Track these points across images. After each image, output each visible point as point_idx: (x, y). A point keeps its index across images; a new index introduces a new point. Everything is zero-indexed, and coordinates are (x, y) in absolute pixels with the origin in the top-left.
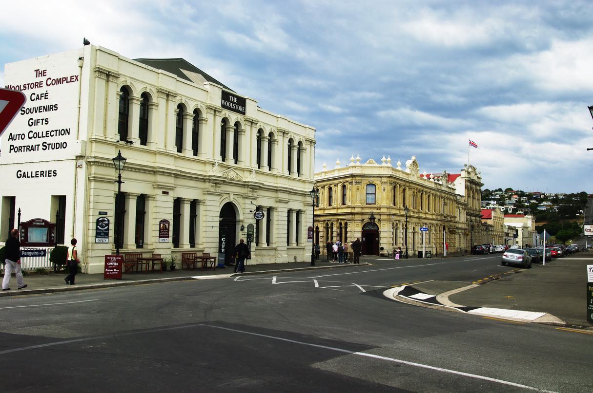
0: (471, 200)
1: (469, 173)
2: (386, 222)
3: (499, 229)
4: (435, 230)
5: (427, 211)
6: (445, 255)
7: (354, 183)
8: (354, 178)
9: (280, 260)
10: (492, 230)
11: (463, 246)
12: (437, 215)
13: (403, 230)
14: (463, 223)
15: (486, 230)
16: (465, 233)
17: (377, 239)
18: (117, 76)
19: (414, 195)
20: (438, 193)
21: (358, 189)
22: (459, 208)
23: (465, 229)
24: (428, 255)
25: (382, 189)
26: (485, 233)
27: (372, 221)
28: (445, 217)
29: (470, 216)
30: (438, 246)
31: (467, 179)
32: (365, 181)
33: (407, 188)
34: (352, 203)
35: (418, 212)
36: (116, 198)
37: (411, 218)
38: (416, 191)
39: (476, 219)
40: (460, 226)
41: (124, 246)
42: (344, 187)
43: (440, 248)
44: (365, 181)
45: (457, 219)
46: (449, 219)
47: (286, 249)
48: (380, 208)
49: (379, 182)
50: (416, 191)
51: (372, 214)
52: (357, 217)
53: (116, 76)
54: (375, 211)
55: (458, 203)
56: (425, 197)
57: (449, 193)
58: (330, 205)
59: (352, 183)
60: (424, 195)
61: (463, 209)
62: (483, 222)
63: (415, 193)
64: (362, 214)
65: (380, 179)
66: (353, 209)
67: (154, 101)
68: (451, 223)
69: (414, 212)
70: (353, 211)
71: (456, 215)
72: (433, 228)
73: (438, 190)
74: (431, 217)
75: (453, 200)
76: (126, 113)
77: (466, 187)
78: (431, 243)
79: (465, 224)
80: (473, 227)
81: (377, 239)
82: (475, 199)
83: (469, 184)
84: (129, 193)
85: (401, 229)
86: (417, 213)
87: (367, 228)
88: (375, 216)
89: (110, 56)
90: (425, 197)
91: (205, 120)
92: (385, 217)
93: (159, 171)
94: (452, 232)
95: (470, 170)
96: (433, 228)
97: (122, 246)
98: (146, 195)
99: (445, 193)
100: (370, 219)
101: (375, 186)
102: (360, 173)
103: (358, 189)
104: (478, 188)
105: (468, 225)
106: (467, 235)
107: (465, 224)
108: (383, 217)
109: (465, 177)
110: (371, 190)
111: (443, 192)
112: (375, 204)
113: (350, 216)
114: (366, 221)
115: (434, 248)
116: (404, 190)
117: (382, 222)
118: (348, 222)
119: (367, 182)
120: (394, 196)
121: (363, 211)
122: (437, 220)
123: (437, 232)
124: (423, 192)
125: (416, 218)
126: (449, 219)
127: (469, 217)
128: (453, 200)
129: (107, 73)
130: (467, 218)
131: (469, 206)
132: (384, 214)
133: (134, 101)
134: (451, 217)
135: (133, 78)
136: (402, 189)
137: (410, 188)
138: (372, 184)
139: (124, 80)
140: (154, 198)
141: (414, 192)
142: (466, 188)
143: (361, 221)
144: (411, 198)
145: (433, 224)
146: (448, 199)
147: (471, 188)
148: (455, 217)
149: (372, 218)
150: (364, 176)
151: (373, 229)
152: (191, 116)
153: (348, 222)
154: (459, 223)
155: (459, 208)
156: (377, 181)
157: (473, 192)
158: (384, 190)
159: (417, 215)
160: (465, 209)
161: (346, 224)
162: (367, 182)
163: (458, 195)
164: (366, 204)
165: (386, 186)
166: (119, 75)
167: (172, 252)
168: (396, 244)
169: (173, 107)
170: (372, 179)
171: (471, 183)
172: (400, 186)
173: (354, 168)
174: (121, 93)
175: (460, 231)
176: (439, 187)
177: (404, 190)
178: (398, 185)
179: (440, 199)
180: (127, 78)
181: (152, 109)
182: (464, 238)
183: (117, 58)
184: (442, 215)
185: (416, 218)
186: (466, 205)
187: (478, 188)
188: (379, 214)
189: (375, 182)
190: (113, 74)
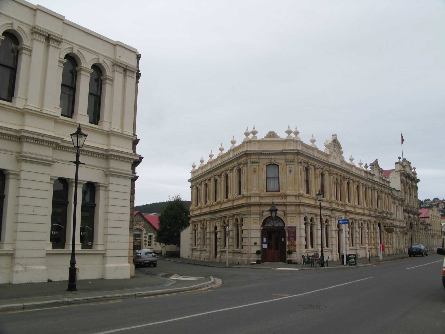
0: (407, 196)
1: (404, 167)
2: (295, 215)
3: (438, 228)
4: (368, 228)
5: (356, 204)
6: (381, 257)
7: (249, 164)
8: (249, 157)
9: (21, 277)
10: (430, 230)
11: (402, 247)
12: (370, 210)
13: (349, 229)
14: (401, 221)
15: (425, 229)
16: (404, 232)
17: (283, 239)
18: (60, 40)
19: (338, 183)
20: (370, 185)
21: (255, 172)
22: (395, 203)
23: (403, 228)
24: (352, 260)
25: (288, 169)
26: (424, 232)
27: (274, 215)
28: (379, 213)
29: (408, 213)
30: (373, 247)
31: (402, 172)
32: (264, 161)
33: (327, 173)
34: (247, 191)
35: (345, 205)
36: (54, 185)
37: (334, 212)
38: (339, 178)
39: (414, 217)
40: (398, 224)
41: (65, 245)
42: (240, 171)
43: (375, 250)
44: (264, 161)
45: (393, 216)
46: (385, 215)
47: (44, 256)
48: (286, 197)
49: (282, 162)
50: (339, 178)
51: (273, 205)
52: (253, 209)
53: (59, 41)
54: (276, 201)
55: (395, 198)
56: (353, 187)
57: (383, 186)
58: (240, 193)
59: (247, 163)
60: (351, 185)
61: (399, 204)
62: (421, 221)
63: (339, 181)
64: (261, 205)
65: (283, 157)
66: (249, 198)
67: (107, 74)
68: (387, 221)
69: (338, 205)
70: (248, 202)
71: (392, 211)
72: (365, 226)
73: (368, 180)
74: (353, 210)
75: (389, 194)
76: (74, 86)
77: (402, 181)
78: (315, 246)
79: (403, 221)
80: (411, 225)
81: (283, 239)
82: (412, 195)
83: (404, 179)
84: (99, 183)
85: (372, 229)
86: (342, 206)
87: (269, 225)
88: (278, 208)
89: (90, 37)
90: (353, 187)
91: (26, 49)
92: (293, 208)
93: (27, 137)
94: (389, 230)
95: (405, 164)
96: (365, 226)
97: (64, 246)
98: (5, 170)
99: (378, 185)
100: (271, 211)
101: (278, 166)
102: (257, 149)
103: (255, 172)
104: (414, 184)
105: (406, 223)
106: (406, 234)
107: (403, 221)
108: (291, 209)
109: (400, 171)
110: (273, 172)
111: (375, 183)
112: (279, 191)
113: (245, 209)
114: (267, 214)
115: (334, 253)
116: (322, 175)
117: (288, 215)
118: (243, 217)
119: (267, 161)
120: (307, 181)
121: (262, 201)
122: (370, 215)
123: (371, 230)
124: (349, 181)
125: (341, 211)
126: (385, 215)
127: (406, 215)
128: (389, 194)
129: (125, 67)
130: (404, 215)
131: (406, 203)
132: (291, 204)
133: (107, 81)
134: (387, 213)
135: (21, 22)
136: (355, 186)
137: (330, 173)
138: (274, 164)
139: (97, 57)
140: (106, 187)
141: (337, 180)
142: (401, 182)
143: (260, 215)
144: (333, 186)
145: (364, 221)
146: (382, 192)
147: (407, 183)
148: (391, 214)
149: (273, 210)
150: (262, 153)
151: (277, 225)
152: (88, 72)
153: (243, 217)
154: (396, 220)
155: (395, 203)
156: (280, 160)
157: (409, 187)
158: (290, 171)
159: (342, 208)
160: (402, 205)
161: (242, 219)
162: (267, 162)
163: (394, 189)
164: (267, 191)
165: (293, 166)
166: (62, 39)
167: (47, 254)
168: (352, 245)
169: (57, 55)
170: (273, 157)
171: (406, 177)
172: (315, 168)
173: (249, 144)
174: (65, 61)
175: (398, 230)
176: (370, 177)
177: (322, 175)
178: (351, 181)
179: (373, 191)
180: (74, 46)
181: (22, 53)
182: (403, 237)
183: (61, 22)
184: (376, 211)
185: (341, 211)
186: (403, 201)
187: (414, 184)
188: (285, 205)
189: (278, 161)
190: (54, 38)
